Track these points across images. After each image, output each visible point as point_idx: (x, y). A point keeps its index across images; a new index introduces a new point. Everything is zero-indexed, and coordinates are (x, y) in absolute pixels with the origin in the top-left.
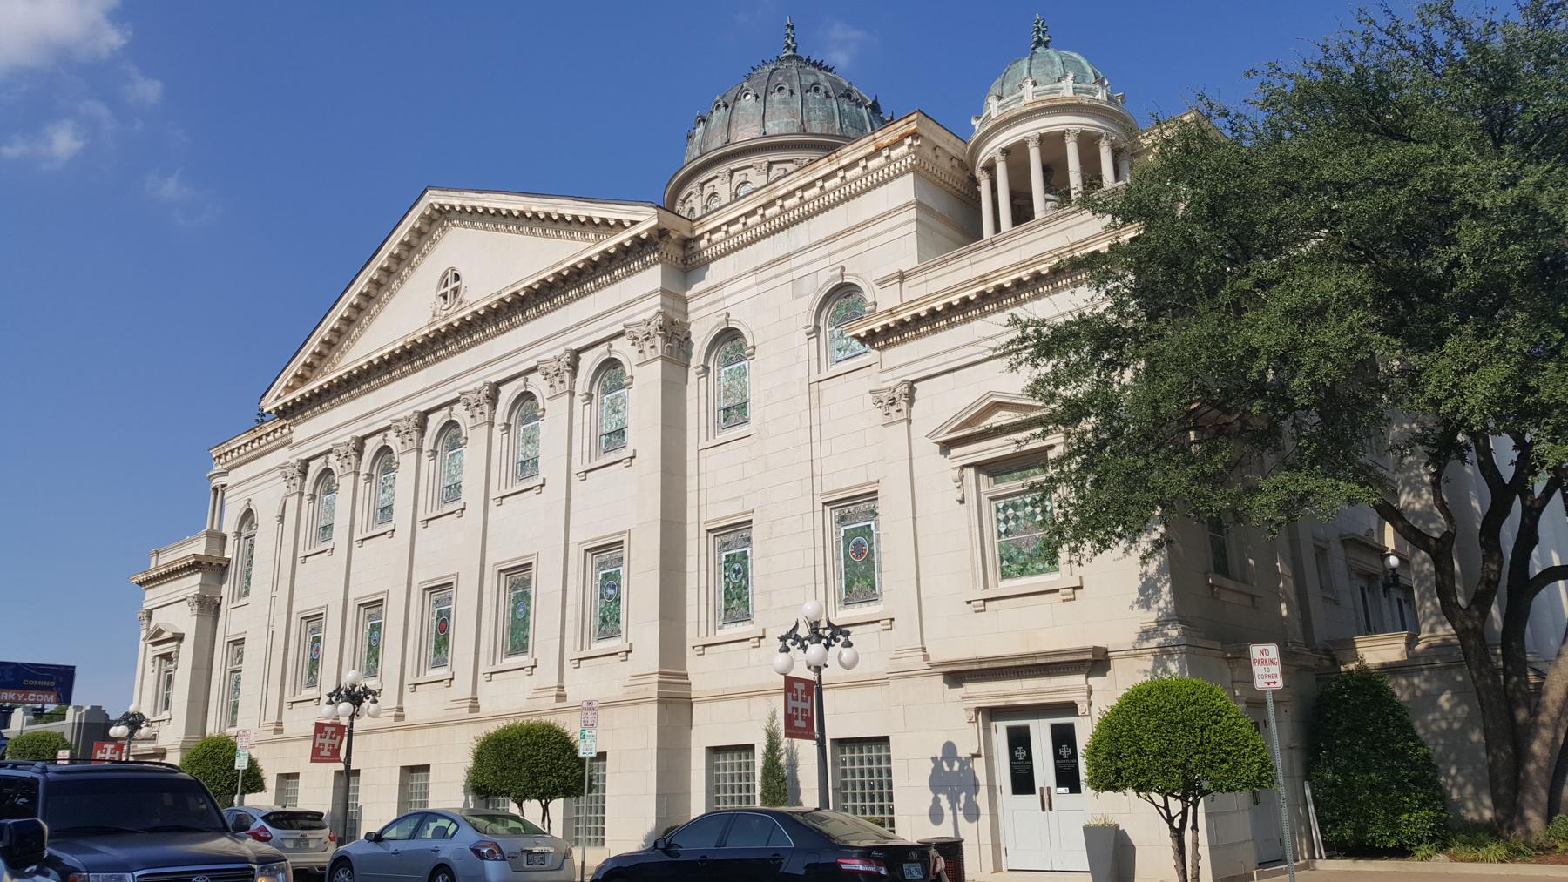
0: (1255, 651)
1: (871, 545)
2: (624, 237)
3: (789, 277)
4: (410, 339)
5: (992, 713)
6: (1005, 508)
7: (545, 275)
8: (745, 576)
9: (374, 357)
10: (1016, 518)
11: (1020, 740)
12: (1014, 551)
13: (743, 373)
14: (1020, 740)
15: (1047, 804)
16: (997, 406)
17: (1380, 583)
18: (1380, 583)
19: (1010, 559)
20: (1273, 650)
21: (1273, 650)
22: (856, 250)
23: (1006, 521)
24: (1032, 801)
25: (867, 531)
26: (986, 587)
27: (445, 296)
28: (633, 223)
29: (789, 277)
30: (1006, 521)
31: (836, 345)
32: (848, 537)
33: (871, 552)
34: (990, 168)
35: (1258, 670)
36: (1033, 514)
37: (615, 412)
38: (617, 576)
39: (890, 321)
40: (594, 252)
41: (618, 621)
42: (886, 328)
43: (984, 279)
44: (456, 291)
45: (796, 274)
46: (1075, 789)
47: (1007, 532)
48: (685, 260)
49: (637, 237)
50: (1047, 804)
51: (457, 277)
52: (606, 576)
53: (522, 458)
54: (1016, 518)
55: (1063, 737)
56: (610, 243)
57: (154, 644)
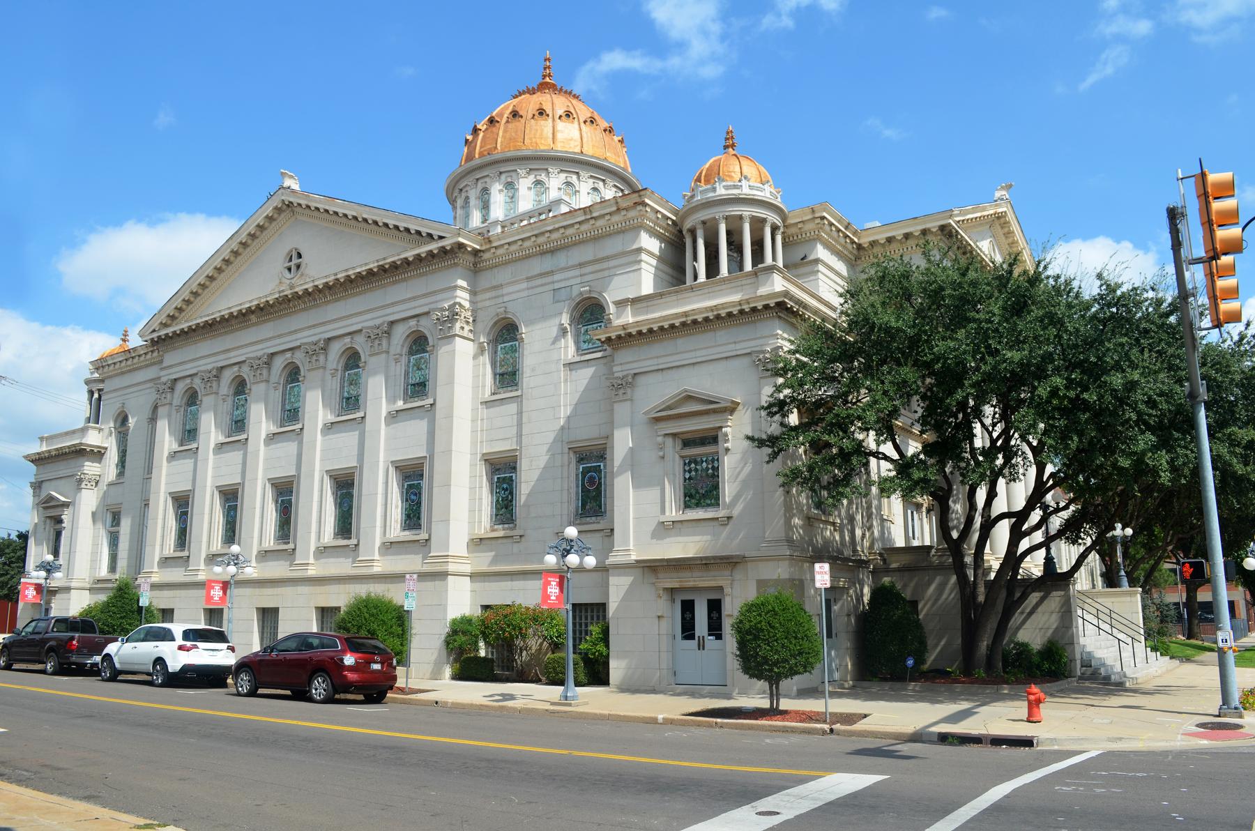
0: (817, 566)
1: (600, 479)
2: (434, 247)
3: (551, 287)
4: (263, 300)
5: (672, 591)
6: (690, 463)
7: (371, 266)
8: (511, 493)
9: (235, 310)
10: (696, 470)
11: (688, 607)
12: (693, 491)
13: (514, 350)
14: (688, 607)
15: (701, 646)
16: (689, 398)
17: (924, 509)
18: (924, 509)
19: (691, 496)
20: (826, 566)
21: (826, 566)
22: (600, 275)
23: (690, 471)
24: (693, 643)
25: (597, 470)
26: (663, 511)
27: (290, 269)
28: (441, 238)
29: (551, 287)
30: (690, 471)
31: (582, 338)
32: (584, 473)
33: (600, 484)
34: (693, 232)
35: (818, 577)
36: (707, 469)
37: (419, 369)
38: (419, 487)
39: (622, 333)
40: (410, 254)
41: (419, 518)
42: (619, 337)
43: (686, 314)
44: (298, 266)
45: (557, 286)
46: (719, 637)
47: (690, 478)
48: (475, 264)
49: (443, 247)
50: (701, 646)
51: (300, 256)
52: (410, 486)
53: (346, 395)
54: (696, 470)
55: (715, 607)
56: (423, 250)
57: (45, 508)
